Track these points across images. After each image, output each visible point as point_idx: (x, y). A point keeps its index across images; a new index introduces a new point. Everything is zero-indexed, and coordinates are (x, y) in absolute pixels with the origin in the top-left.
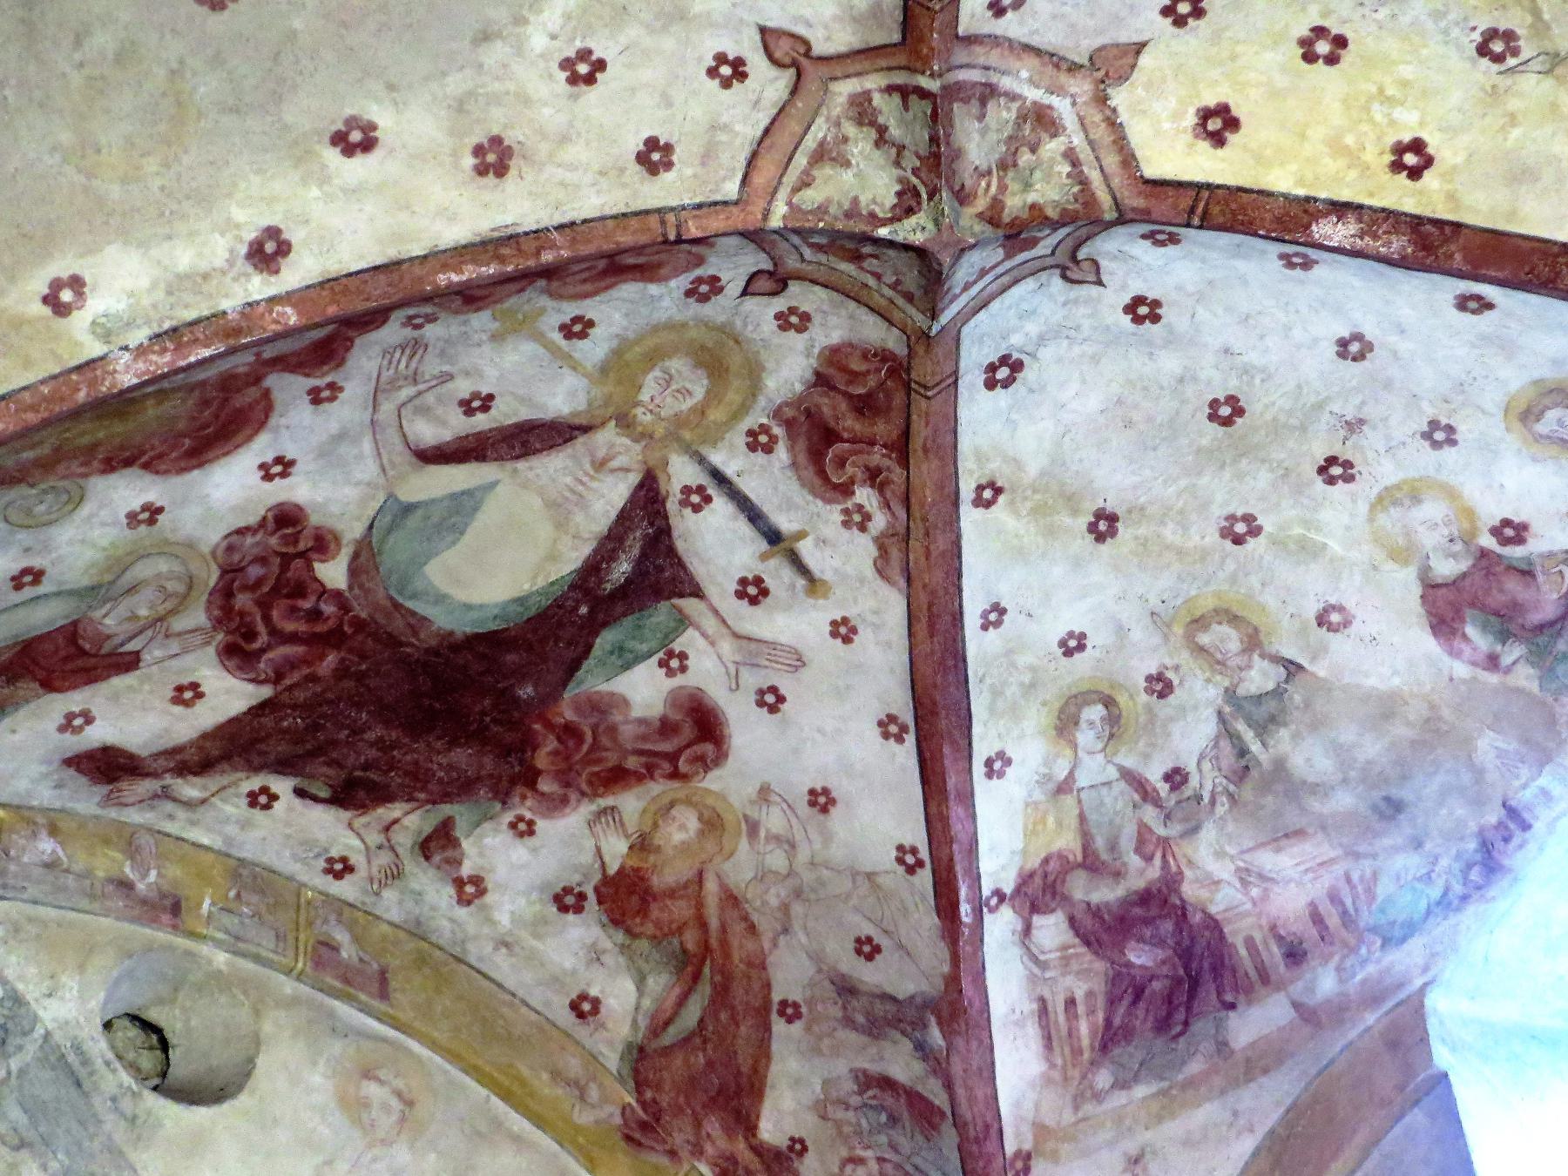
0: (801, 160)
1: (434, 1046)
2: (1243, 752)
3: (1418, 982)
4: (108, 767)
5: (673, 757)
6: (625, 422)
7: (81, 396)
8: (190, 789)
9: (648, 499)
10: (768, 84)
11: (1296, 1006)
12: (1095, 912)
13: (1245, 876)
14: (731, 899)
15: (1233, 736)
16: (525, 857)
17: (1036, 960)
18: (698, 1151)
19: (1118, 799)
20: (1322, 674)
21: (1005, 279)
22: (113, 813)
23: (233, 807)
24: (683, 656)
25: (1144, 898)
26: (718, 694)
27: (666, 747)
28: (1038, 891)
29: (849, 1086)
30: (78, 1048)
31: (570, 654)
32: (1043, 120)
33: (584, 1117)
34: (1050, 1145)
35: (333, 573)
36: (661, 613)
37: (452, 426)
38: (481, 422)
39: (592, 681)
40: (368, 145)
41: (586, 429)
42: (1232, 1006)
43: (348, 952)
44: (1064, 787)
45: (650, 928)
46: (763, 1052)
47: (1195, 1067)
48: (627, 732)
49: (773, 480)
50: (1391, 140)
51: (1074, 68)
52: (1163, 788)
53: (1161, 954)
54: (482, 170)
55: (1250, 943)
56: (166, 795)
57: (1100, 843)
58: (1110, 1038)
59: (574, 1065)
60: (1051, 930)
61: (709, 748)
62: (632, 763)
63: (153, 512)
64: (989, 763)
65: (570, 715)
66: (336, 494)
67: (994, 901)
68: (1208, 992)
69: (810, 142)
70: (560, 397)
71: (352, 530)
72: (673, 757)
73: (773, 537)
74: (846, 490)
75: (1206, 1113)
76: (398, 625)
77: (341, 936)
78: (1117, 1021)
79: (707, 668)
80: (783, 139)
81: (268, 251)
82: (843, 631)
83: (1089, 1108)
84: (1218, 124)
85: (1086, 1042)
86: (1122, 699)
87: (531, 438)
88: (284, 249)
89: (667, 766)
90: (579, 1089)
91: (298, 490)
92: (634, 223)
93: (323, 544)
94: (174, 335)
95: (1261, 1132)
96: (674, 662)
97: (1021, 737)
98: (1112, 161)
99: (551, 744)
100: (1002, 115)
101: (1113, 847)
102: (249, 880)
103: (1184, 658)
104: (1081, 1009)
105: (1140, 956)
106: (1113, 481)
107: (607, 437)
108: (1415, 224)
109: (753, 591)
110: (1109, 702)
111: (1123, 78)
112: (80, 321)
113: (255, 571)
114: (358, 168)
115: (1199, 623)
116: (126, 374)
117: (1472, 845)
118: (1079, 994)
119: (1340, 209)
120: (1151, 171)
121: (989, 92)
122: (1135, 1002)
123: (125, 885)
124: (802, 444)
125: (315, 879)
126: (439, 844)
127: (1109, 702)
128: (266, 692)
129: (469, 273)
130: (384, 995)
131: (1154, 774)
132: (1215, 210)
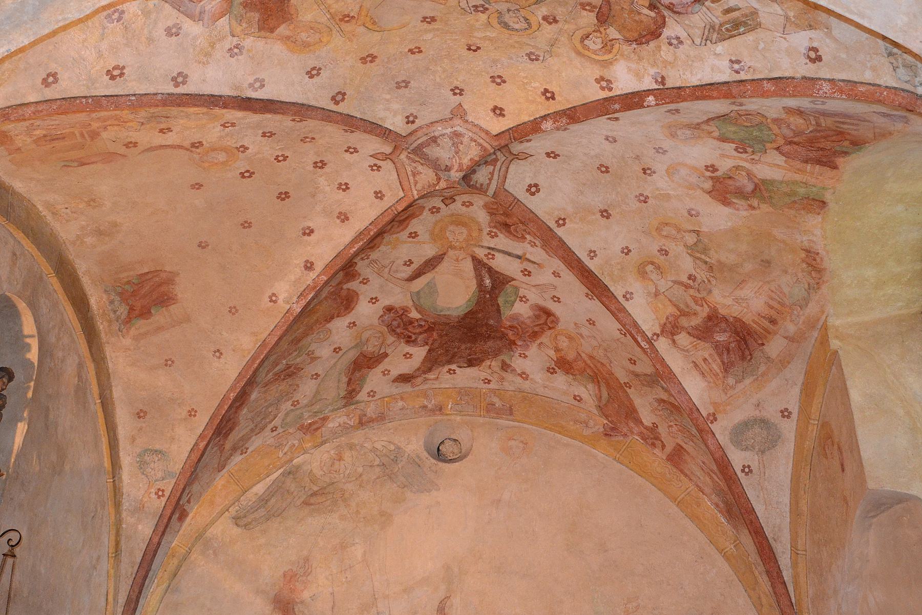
0: (411, 178)
1: (532, 424)
2: (706, 263)
3: (824, 318)
4: (404, 379)
5: (546, 323)
6: (452, 247)
7: (291, 318)
8: (431, 376)
9: (478, 263)
10: (387, 165)
12: (696, 328)
13: (737, 300)
15: (699, 259)
16: (532, 362)
17: (684, 350)
18: (632, 433)
19: (679, 291)
20: (706, 230)
21: (503, 169)
22: (417, 388)
23: (448, 376)
24: (524, 297)
25: (710, 318)
26: (542, 303)
28: (671, 329)
29: (656, 404)
30: (418, 457)
31: (495, 308)
32: (457, 134)
33: (587, 432)
34: (721, 408)
35: (414, 315)
36: (509, 288)
38: (415, 266)
39: (506, 313)
40: (312, 231)
41: (445, 254)
42: (763, 344)
43: (498, 404)
44: (657, 294)
45: (577, 372)
46: (630, 400)
47: (763, 368)
48: (528, 321)
49: (503, 241)
50: (539, 93)
51: (451, 119)
52: (691, 282)
53: (728, 334)
54: (343, 221)
55: (753, 321)
56: (426, 379)
57: (682, 306)
58: (727, 368)
59: (583, 416)
60: (683, 339)
61: (552, 318)
62: (536, 329)
64: (624, 296)
65: (508, 323)
66: (398, 297)
67: (655, 337)
68: (751, 342)
69: (410, 173)
70: (430, 251)
72: (546, 323)
73: (519, 257)
74: (524, 238)
75: (774, 384)
76: (444, 320)
77: (496, 400)
78: (726, 361)
79: (534, 297)
80: (403, 175)
81: (309, 266)
82: (556, 274)
83: (731, 392)
84: (498, 111)
85: (718, 371)
86: (656, 261)
87: (431, 264)
88: (312, 264)
89: (546, 327)
91: (386, 301)
92: (386, 214)
93: (405, 310)
95: (800, 384)
97: (631, 284)
98: (483, 135)
99: (510, 333)
100: (446, 142)
101: (688, 306)
102: (464, 393)
103: (663, 241)
104: (710, 361)
105: (721, 337)
106: (597, 201)
107: (451, 253)
108: (563, 113)
109: (527, 273)
110: (652, 263)
111: (466, 114)
112: (280, 301)
113: (395, 323)
114: (313, 237)
115: (658, 229)
116: (298, 309)
117: (804, 265)
118: (707, 356)
119: (544, 117)
120: (494, 133)
121: (434, 140)
122: (728, 353)
123: (425, 407)
124: (504, 231)
126: (505, 367)
127: (652, 263)
128: (427, 348)
129: (357, 246)
130: (511, 414)
131: (684, 278)
132: (516, 135)
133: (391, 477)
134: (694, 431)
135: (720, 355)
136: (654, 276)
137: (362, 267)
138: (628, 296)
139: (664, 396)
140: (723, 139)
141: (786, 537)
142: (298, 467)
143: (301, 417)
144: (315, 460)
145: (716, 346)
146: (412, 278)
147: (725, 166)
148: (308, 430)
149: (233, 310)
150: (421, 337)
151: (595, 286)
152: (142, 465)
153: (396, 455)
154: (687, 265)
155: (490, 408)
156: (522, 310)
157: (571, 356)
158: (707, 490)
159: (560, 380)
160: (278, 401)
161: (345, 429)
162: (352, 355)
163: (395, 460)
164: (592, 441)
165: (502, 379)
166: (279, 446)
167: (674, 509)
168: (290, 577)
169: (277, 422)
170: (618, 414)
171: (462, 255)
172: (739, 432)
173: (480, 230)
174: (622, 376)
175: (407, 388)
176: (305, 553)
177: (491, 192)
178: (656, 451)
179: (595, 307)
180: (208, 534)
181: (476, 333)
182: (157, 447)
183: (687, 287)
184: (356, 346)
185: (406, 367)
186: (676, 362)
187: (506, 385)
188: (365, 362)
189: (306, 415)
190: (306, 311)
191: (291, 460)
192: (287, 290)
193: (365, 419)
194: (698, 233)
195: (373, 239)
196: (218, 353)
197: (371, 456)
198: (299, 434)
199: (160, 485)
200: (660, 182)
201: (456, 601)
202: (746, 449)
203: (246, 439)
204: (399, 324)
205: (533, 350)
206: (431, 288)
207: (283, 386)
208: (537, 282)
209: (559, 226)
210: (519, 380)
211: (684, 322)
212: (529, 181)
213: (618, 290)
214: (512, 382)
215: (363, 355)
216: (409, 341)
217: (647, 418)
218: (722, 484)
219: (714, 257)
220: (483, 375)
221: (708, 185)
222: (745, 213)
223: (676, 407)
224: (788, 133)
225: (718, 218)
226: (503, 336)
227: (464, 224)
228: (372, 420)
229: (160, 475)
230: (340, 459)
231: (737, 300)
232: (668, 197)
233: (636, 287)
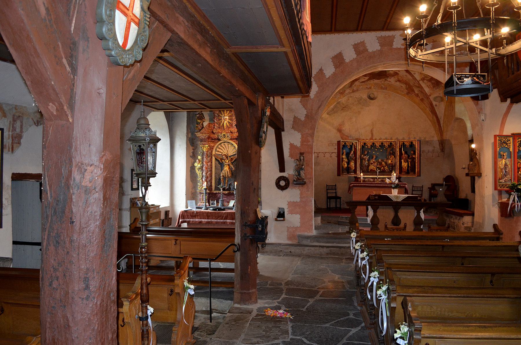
28: (423, 79)
58: (434, 87)
60: (425, 81)
141: (442, 119)
144: (343, 100)
145: (432, 83)
155: (382, 88)
159: (398, 83)
161: (350, 93)
168: (340, 125)
172: (435, 99)
174: (411, 84)
186: (423, 85)
201: (375, 129)
213: (413, 73)
214: (386, 82)
217: (416, 92)
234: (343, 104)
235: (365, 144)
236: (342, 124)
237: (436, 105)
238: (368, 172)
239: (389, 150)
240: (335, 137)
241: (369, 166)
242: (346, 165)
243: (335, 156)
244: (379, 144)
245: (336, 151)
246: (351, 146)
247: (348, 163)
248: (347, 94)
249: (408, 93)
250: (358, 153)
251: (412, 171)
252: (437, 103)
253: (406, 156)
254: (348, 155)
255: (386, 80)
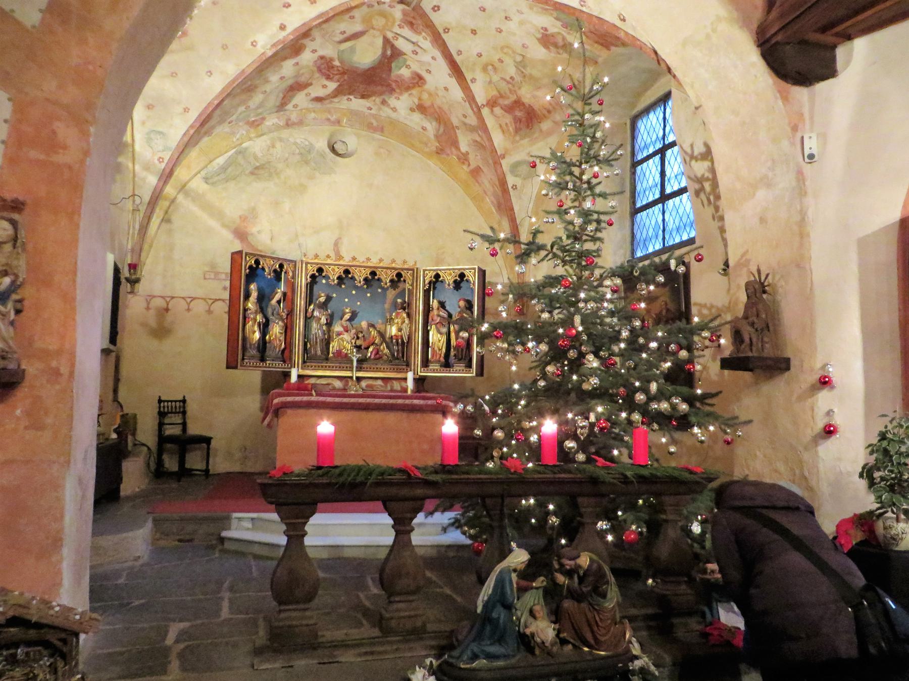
4: (319, 99)
8: (336, 100)
9: (386, 41)
11: (554, 122)
14: (440, 108)
23: (346, 102)
26: (419, 72)
27: (415, 81)
28: (492, 104)
35: (337, 63)
36: (401, 59)
37: (342, 37)
38: (345, 35)
43: (375, 124)
46: (456, 137)
47: (536, 135)
49: (406, 32)
56: (331, 102)
58: (517, 130)
59: (425, 139)
60: (498, 110)
63: (297, 64)
66: (329, 51)
70: (358, 28)
71: (336, 56)
73: (413, 43)
79: (415, 67)
81: (283, 27)
82: (433, 58)
87: (356, 36)
90: (426, 144)
91: (321, 53)
93: (331, 60)
94: (274, 45)
96: (408, 67)
102: (354, 113)
105: (519, 114)
114: (290, 9)
115: (502, 48)
116: (270, 53)
123: (328, 120)
125: (365, 110)
126: (384, 102)
131: (508, 78)
133: (307, 162)
134: (491, 161)
135: (515, 123)
136: (491, 73)
137: (316, 33)
138: (473, 80)
139: (478, 139)
140: (557, 19)
142: (246, 149)
143: (249, 116)
144: (257, 146)
146: (341, 42)
147: (552, 30)
148: (254, 124)
149: (225, 47)
150: (337, 77)
151: (456, 70)
152: (149, 140)
153: (310, 149)
154: (512, 71)
155: (371, 127)
156: (405, 73)
157: (427, 103)
158: (489, 193)
160: (239, 105)
161: (278, 128)
162: (290, 82)
163: (309, 152)
164: (429, 155)
165: (380, 109)
166: (233, 134)
167: (468, 201)
168: (243, 218)
169: (234, 117)
170: (447, 140)
171: (377, 33)
172: (515, 166)
173: (394, 22)
174: (455, 121)
175: (318, 105)
176: (253, 204)
177: (412, 6)
178: (465, 167)
179: (453, 83)
180: (187, 187)
181: (374, 80)
182: (160, 129)
183: (508, 83)
184: (296, 76)
185: (321, 93)
186: (490, 122)
187: (382, 113)
188: (297, 87)
189: (252, 115)
190: (275, 55)
191: (241, 144)
192: (266, 40)
193: (290, 123)
194: (523, 56)
195: (328, 19)
196: (210, 73)
197: (294, 147)
198: (246, 127)
199: (161, 155)
200: (512, 25)
201: (345, 241)
202: (516, 176)
203: (213, 127)
204: (325, 67)
205: (405, 97)
206: (352, 50)
207: (244, 97)
208: (420, 56)
209: (445, 32)
210: (389, 111)
211: (501, 101)
212: (435, 3)
213: (468, 76)
214: (386, 112)
215: (297, 83)
216: (328, 78)
217: (464, 147)
218: (500, 193)
219: (528, 71)
220: (368, 105)
221: (539, 36)
222: (553, 55)
223: (486, 146)
224: (591, 27)
225: (539, 52)
226: (389, 85)
227: (385, 17)
228: (294, 124)
229: (161, 148)
230: (273, 146)
231: (534, 97)
232: (515, 34)
233: (480, 76)
234: (256, 158)
235: (320, 270)
236: (251, 215)
237: (515, 187)
238: (327, 359)
239: (391, 294)
240: (222, 246)
241: (327, 342)
242: (257, 336)
243: (221, 309)
244: (366, 273)
245: (226, 295)
246: (277, 275)
247: (265, 327)
248: (270, 131)
249: (440, 152)
250: (300, 302)
251: (459, 359)
252: (518, 181)
253: (443, 314)
254: (263, 299)
255: (384, 102)
